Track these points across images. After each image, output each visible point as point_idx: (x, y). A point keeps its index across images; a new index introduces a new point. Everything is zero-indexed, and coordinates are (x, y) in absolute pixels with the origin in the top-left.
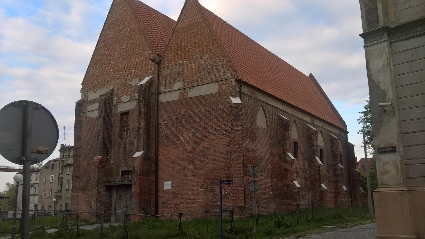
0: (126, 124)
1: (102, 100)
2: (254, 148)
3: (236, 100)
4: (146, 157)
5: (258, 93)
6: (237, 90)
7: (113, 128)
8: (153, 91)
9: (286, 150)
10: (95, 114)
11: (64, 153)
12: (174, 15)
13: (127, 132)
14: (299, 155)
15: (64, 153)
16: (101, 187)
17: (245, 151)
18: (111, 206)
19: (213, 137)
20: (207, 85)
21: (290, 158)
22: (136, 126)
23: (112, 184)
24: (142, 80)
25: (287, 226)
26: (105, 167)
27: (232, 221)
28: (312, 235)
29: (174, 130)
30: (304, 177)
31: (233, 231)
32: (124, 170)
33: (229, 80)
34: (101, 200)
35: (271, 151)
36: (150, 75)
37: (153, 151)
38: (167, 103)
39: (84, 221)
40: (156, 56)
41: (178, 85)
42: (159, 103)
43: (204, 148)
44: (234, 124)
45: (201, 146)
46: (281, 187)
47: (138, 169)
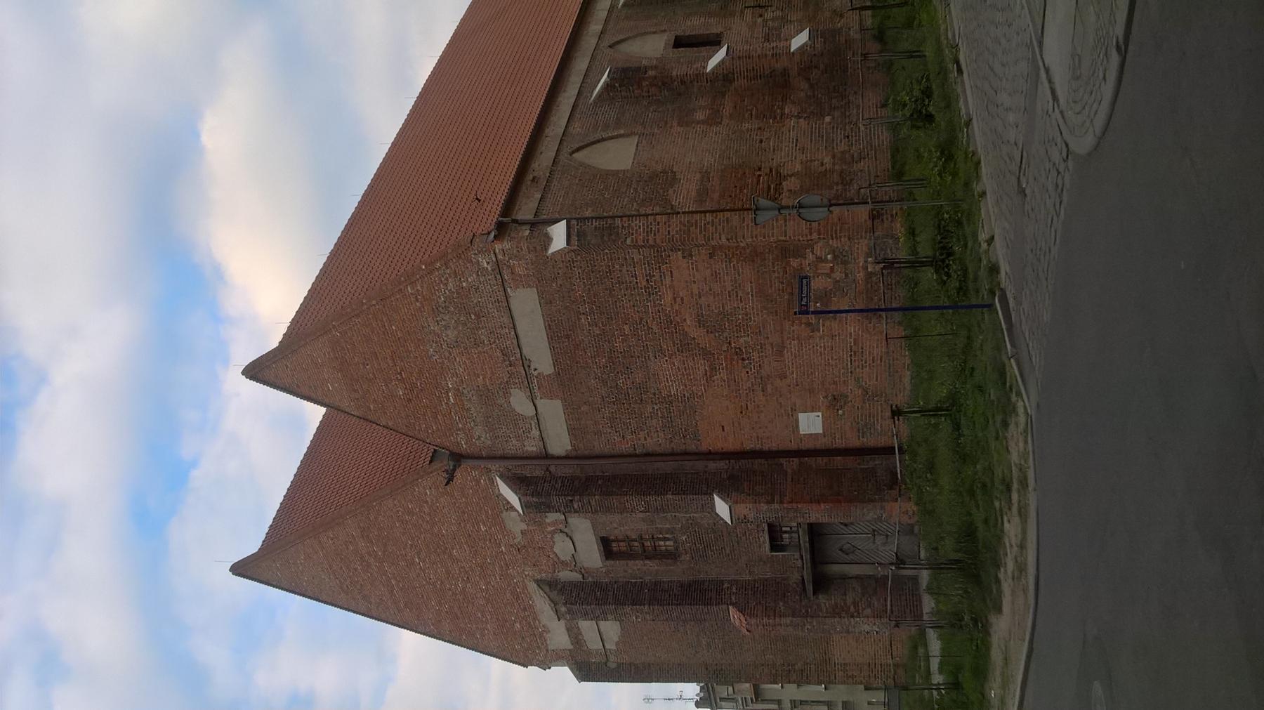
0: (636, 544)
1: (569, 611)
2: (698, 176)
3: (558, 235)
4: (729, 487)
5: (535, 165)
6: (527, 233)
7: (647, 578)
8: (538, 473)
9: (699, 76)
10: (611, 629)
11: (722, 699)
12: (315, 414)
13: (660, 539)
14: (715, 30)
15: (722, 699)
16: (819, 605)
17: (708, 206)
18: (870, 577)
19: (668, 298)
20: (516, 318)
21: (723, 61)
22: (641, 515)
23: (807, 574)
24: (508, 503)
25: (927, 93)
26: (761, 596)
27: (915, 264)
28: (952, 26)
29: (649, 409)
30: (778, 13)
31: (943, 261)
32: (767, 545)
33: (500, 257)
34: (855, 604)
35: (703, 122)
36: (492, 482)
37: (712, 465)
38: (572, 431)
39: (915, 647)
40: (436, 465)
41: (520, 402)
42: (574, 453)
43: (701, 323)
44: (629, 241)
45: (695, 333)
46: (811, 86)
47: (764, 507)
